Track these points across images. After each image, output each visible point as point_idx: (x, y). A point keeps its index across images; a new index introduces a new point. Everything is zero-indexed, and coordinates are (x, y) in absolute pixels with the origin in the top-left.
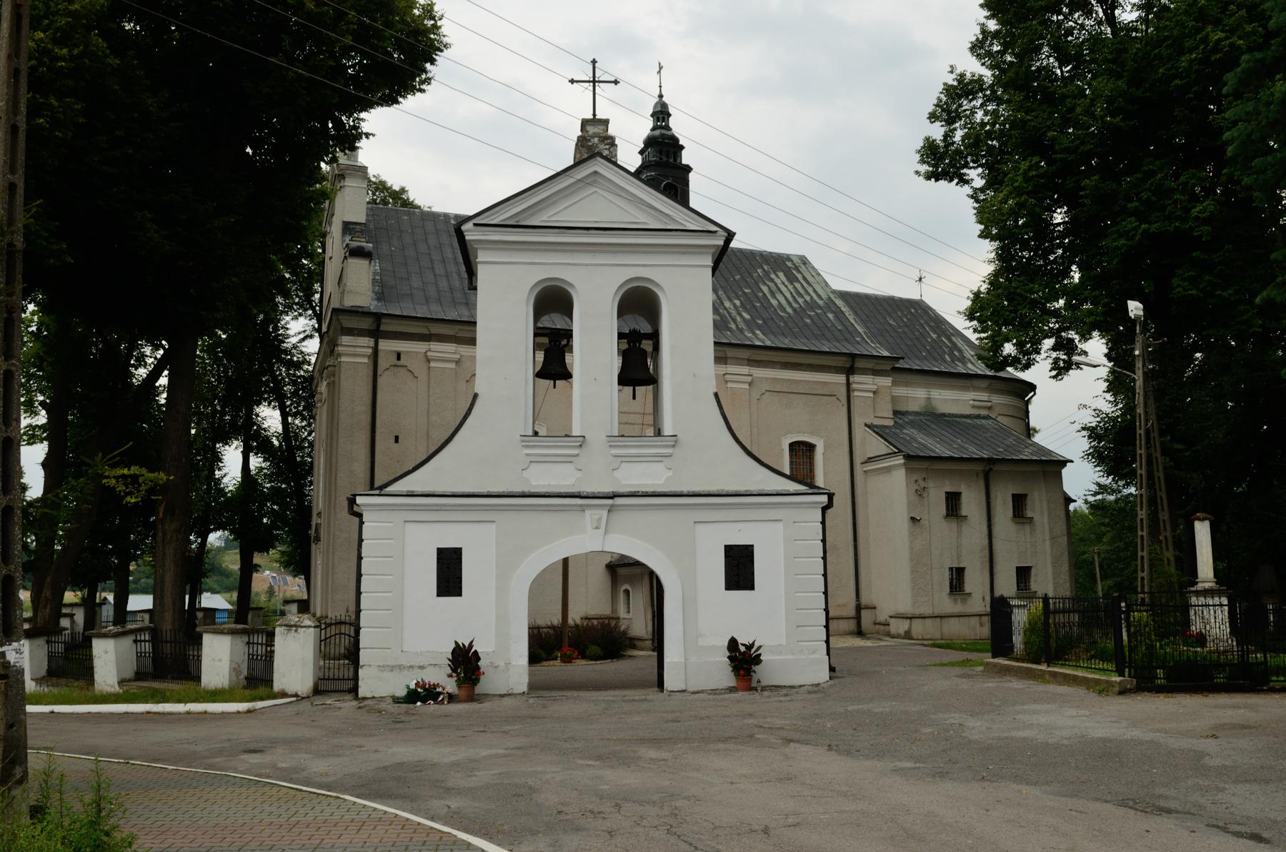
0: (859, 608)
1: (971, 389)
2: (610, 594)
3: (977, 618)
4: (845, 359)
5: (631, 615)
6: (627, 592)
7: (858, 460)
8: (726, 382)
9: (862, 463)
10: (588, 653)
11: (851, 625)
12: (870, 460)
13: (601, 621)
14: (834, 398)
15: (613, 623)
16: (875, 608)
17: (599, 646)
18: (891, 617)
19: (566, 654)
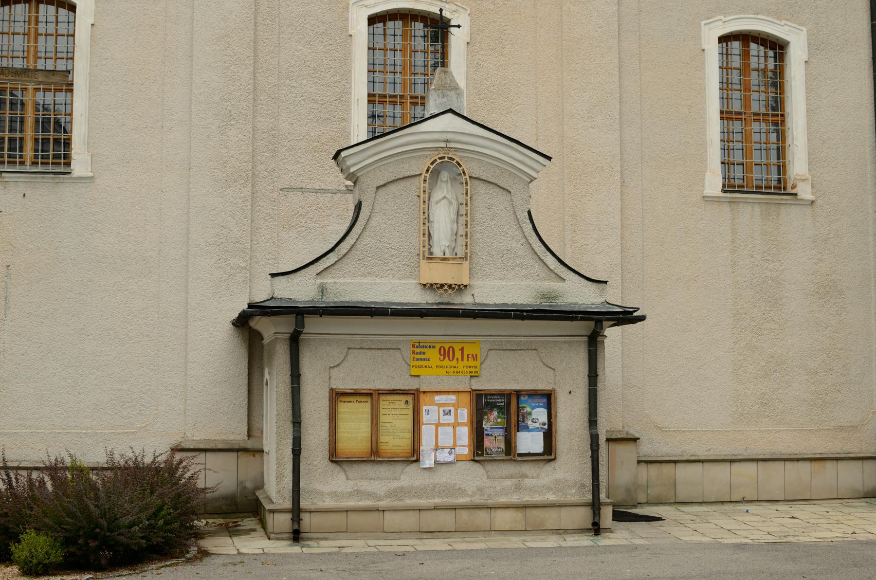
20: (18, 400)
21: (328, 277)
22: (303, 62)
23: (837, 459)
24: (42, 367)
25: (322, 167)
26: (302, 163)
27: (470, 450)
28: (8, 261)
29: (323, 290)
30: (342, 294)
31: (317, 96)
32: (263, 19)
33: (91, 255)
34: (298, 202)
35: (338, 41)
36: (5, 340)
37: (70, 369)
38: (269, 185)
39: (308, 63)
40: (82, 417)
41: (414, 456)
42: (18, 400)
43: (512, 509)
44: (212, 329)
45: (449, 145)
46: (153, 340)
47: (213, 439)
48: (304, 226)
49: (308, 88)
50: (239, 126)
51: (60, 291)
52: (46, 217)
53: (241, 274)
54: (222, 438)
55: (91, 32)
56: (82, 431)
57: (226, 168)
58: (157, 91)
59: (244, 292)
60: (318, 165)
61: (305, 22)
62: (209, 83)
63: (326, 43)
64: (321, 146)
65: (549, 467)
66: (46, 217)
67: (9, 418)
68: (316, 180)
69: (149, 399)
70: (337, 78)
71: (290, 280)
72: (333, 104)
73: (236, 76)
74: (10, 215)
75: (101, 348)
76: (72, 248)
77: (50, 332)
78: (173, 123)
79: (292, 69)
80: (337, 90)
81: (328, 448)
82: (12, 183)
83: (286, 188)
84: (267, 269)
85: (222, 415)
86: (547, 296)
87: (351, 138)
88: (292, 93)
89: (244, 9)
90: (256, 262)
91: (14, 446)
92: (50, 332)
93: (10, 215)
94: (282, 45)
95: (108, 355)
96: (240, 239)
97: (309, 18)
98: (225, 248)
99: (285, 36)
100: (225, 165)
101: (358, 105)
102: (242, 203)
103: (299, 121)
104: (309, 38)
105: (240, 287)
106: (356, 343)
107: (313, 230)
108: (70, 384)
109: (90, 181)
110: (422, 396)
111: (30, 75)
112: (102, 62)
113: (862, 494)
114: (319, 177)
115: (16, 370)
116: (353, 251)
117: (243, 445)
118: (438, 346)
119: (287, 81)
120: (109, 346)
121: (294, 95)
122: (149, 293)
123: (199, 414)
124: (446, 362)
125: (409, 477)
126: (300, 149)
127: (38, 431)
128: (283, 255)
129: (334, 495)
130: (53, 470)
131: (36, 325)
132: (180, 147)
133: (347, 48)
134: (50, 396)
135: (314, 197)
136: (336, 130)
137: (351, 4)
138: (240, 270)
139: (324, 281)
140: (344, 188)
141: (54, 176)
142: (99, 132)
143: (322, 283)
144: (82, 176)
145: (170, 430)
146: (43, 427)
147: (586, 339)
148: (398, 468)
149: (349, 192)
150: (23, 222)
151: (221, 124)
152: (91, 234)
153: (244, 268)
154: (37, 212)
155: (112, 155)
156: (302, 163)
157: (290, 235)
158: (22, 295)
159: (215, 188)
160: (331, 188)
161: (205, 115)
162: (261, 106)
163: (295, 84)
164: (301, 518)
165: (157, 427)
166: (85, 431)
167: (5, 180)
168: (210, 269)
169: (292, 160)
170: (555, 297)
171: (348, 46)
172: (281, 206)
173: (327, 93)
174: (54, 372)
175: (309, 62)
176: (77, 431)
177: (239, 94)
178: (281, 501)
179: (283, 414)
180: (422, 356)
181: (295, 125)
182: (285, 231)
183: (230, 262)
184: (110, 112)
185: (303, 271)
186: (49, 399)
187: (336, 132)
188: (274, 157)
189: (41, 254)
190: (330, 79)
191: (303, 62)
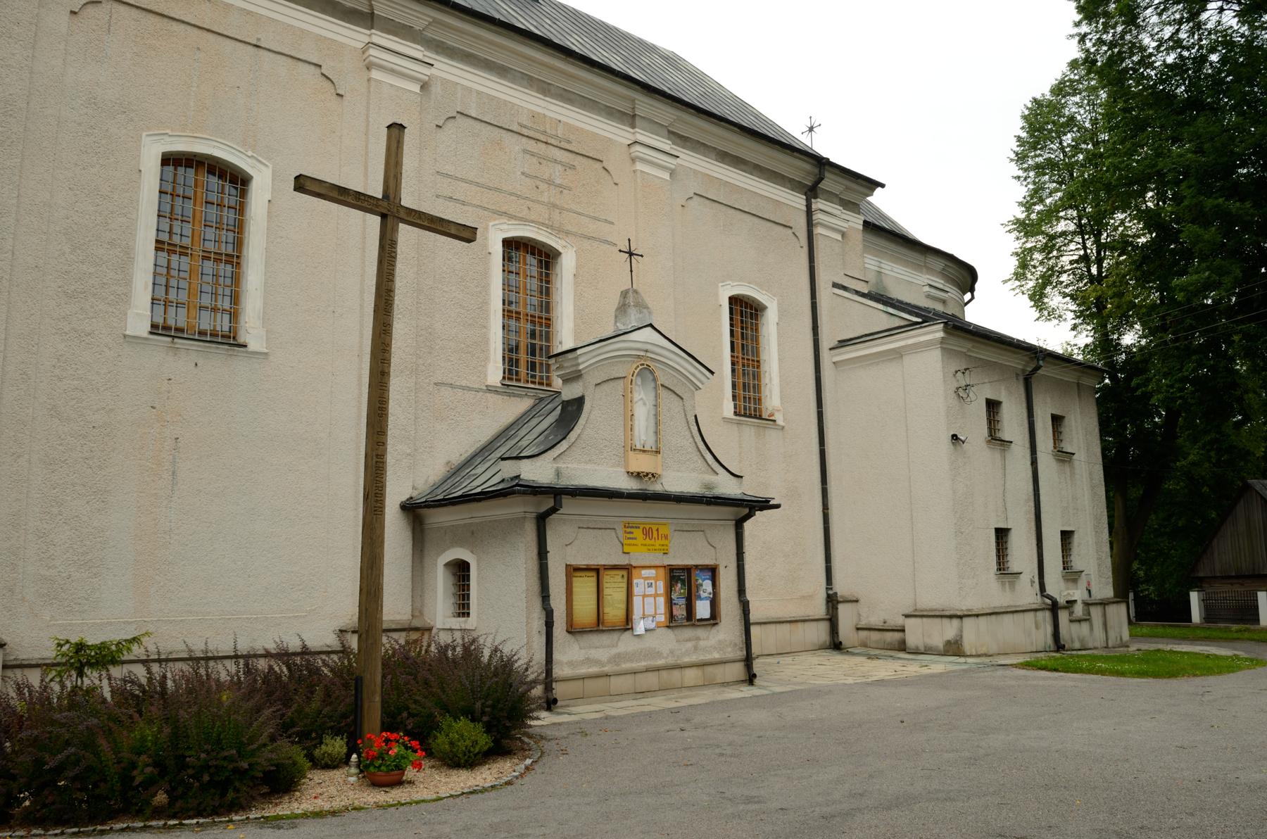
0: (832, 601)
1: (924, 270)
3: (1031, 614)
4: (807, 167)
5: (471, 622)
6: (461, 570)
7: (826, 342)
8: (633, 160)
9: (830, 349)
11: (820, 632)
12: (843, 343)
14: (790, 231)
16: (857, 601)
18: (907, 616)
23: (804, 621)
24: (212, 548)
25: (467, 366)
27: (666, 618)
39: (457, 272)
41: (627, 624)
43: (695, 668)
45: (649, 355)
55: (269, 208)
65: (715, 629)
70: (478, 289)
74: (181, 383)
86: (708, 486)
93: (181, 383)
110: (634, 571)
113: (817, 648)
118: (642, 526)
119: (440, 286)
124: (648, 541)
125: (625, 643)
129: (570, 663)
130: (283, 655)
137: (490, 227)
140: (485, 388)
147: (734, 522)
148: (615, 636)
153: (410, 455)
167: (176, 346)
170: (713, 488)
180: (631, 536)
188: (430, 353)
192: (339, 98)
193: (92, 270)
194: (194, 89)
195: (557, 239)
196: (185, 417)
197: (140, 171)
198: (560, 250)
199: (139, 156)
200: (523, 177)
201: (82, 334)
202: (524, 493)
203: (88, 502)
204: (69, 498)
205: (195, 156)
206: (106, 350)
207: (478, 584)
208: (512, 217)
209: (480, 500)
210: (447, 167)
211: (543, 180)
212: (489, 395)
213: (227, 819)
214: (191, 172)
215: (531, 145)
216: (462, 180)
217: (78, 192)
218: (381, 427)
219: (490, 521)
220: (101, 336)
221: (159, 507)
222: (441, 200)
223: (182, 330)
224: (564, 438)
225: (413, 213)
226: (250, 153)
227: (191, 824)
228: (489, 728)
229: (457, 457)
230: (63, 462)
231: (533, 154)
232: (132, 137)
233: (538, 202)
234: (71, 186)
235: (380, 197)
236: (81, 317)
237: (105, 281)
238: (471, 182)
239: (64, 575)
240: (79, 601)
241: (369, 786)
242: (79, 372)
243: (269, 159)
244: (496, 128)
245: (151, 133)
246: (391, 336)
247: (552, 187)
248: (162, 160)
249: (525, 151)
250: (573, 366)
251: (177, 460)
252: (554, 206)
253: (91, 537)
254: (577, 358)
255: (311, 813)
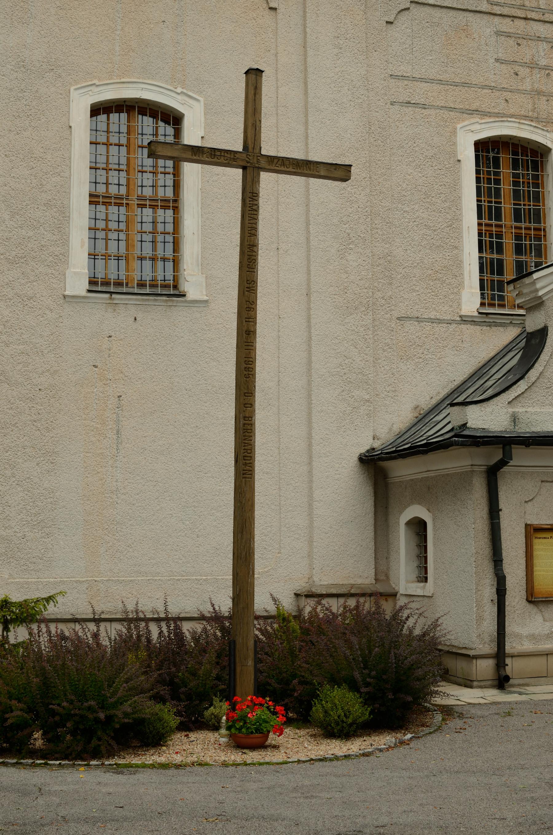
2: (372, 521)
5: (429, 588)
10: (317, 711)
13: (352, 603)
15: (387, 608)
17: (354, 686)
19: (244, 719)
20: (133, 543)
21: (518, 406)
22: (414, 186)
26: (418, 291)
28: (119, 391)
29: (515, 419)
30: (533, 423)
31: (429, 222)
32: (374, 139)
33: (207, 385)
34: (414, 332)
35: (447, 166)
36: (118, 478)
37: (187, 510)
38: (387, 314)
39: (419, 188)
40: (202, 562)
42: (133, 543)
44: (337, 465)
46: (273, 477)
47: (341, 583)
48: (421, 358)
49: (420, 213)
50: (358, 250)
51: (176, 424)
52: (159, 343)
53: (364, 407)
54: (349, 582)
56: (201, 578)
57: (346, 294)
58: (271, 210)
59: (368, 426)
60: (433, 294)
61: (415, 145)
62: (326, 204)
63: (436, 168)
64: (434, 274)
66: (159, 343)
67: (124, 564)
68: (431, 310)
69: (270, 541)
70: (447, 204)
71: (483, 409)
72: (445, 231)
73: (353, 198)
74: (121, 340)
75: (220, 486)
76: (187, 378)
77: (166, 470)
78: (289, 245)
79: (404, 193)
80: (448, 216)
81: (525, 587)
82: (122, 305)
83: (402, 317)
84: (387, 402)
85: (349, 557)
87: (464, 266)
88: (405, 218)
89: (359, 127)
90: (376, 394)
91: (130, 595)
92: (166, 470)
93: (121, 340)
94: (393, 168)
95: (227, 494)
96: (363, 370)
97: (418, 140)
98: (349, 379)
99: (396, 159)
100: (346, 291)
101: (469, 232)
102: (364, 332)
103: (413, 247)
104: (419, 162)
105: (364, 421)
106: (549, 475)
107: (430, 362)
108: (188, 527)
109: (204, 306)
111: (312, 168)
112: (213, 178)
114: (434, 306)
115: (131, 511)
116: (541, 379)
117: (374, 589)
120: (229, 484)
121: (407, 220)
122: (269, 427)
123: (326, 557)
126: (414, 277)
127: (155, 578)
128: (402, 387)
129: (533, 637)
131: (151, 462)
132: (297, 271)
133: (456, 173)
134: (167, 540)
135: (430, 327)
136: (448, 258)
137: (458, 129)
138: (364, 403)
139: (517, 410)
140: (458, 319)
141: (167, 299)
142: (212, 252)
143: (514, 412)
144: (198, 299)
145: (293, 574)
146: (159, 573)
149: (464, 322)
150: (134, 348)
151: (340, 248)
152: (206, 362)
153: (368, 401)
154: (149, 338)
155: (226, 278)
156: (418, 291)
157: (408, 366)
158: (135, 428)
159: (336, 315)
160: (445, 318)
161: (324, 237)
162: (376, 231)
163: (407, 209)
164: (506, 663)
165: (280, 572)
166: (205, 578)
167: (115, 302)
168: (334, 401)
169: (408, 288)
171: (456, 171)
172: (398, 336)
173: (439, 220)
174: (171, 513)
175: (420, 187)
176: (196, 577)
177: (357, 217)
178: (481, 646)
179: (481, 553)
181: (409, 252)
182: (403, 362)
183: (353, 394)
184: (223, 231)
185: (495, 400)
186: (167, 543)
187: (449, 260)
188: (391, 284)
189: (155, 384)
190: (441, 204)
191: (414, 186)
192: (272, 13)
193: (31, 234)
194: (118, 33)
195: (545, 133)
196: (126, 374)
197: (70, 127)
198: (549, 145)
199: (69, 112)
200: (497, 64)
201: (25, 299)
202: (463, 444)
203: (38, 464)
204: (20, 461)
205: (125, 101)
206: (47, 312)
207: (434, 545)
208: (484, 114)
209: (425, 452)
210: (402, 68)
211: (524, 65)
212: (464, 327)
213: (86, 763)
214: (124, 116)
215: (506, 25)
216: (422, 80)
217: (13, 158)
218: (248, 388)
219: (443, 476)
220: (42, 299)
221: (105, 467)
222: (397, 107)
223: (119, 284)
224: (522, 378)
225: (276, 161)
226: (179, 90)
227: (54, 765)
228: (368, 700)
229: (426, 403)
230: (14, 425)
231: (509, 35)
232: (61, 94)
233: (518, 91)
234: (7, 153)
235: (241, 150)
236: (23, 282)
237: (43, 243)
238: (431, 81)
239: (18, 535)
240: (34, 560)
241: (234, 747)
242: (24, 337)
243: (200, 92)
244: (461, 12)
245: (79, 86)
246: (256, 294)
247: (536, 71)
248: (91, 111)
249: (499, 33)
250: (532, 292)
251: (121, 419)
252: (539, 93)
253: (42, 498)
254: (534, 283)
255: (159, 764)
